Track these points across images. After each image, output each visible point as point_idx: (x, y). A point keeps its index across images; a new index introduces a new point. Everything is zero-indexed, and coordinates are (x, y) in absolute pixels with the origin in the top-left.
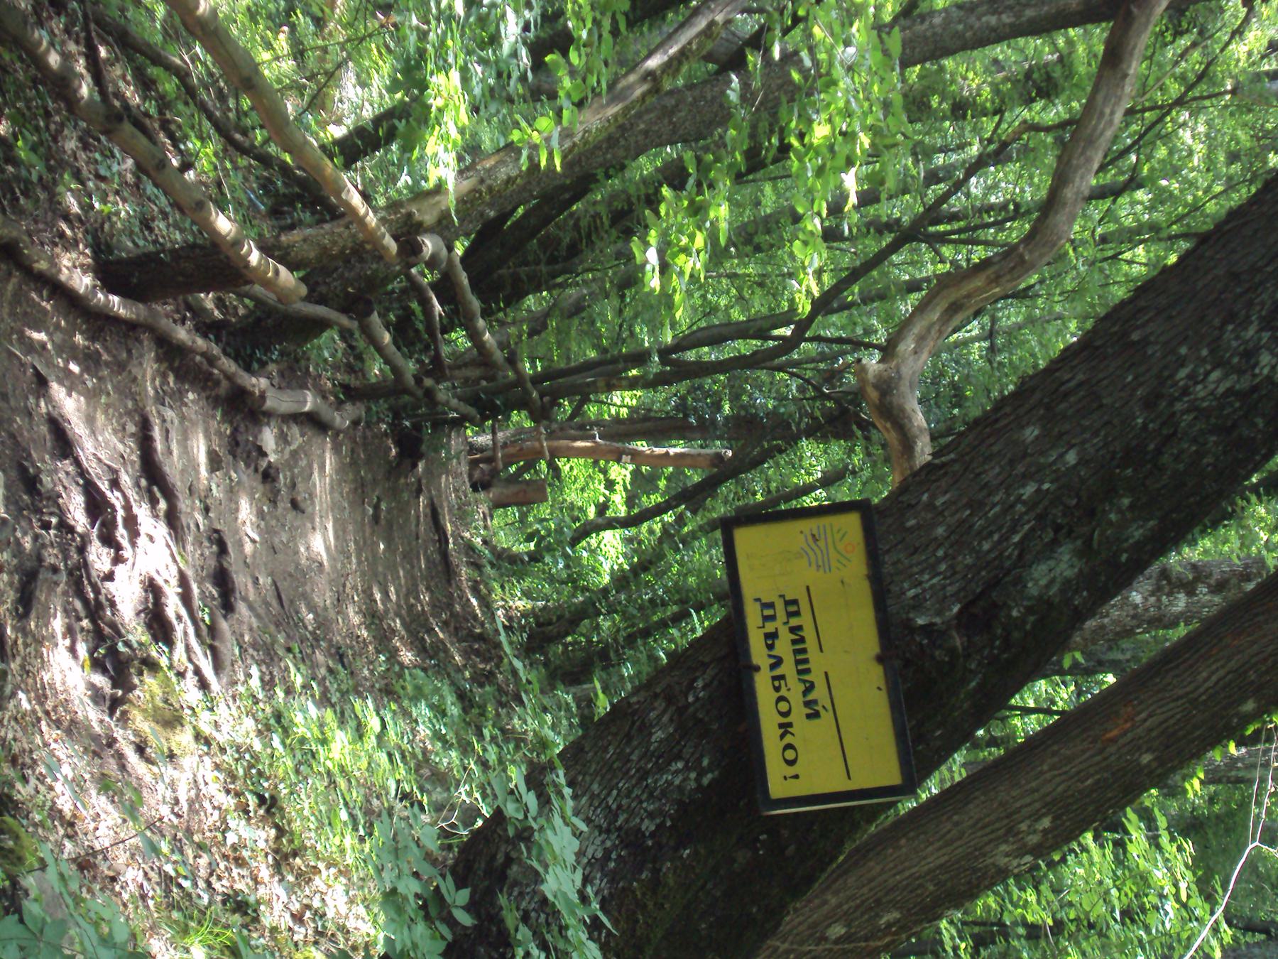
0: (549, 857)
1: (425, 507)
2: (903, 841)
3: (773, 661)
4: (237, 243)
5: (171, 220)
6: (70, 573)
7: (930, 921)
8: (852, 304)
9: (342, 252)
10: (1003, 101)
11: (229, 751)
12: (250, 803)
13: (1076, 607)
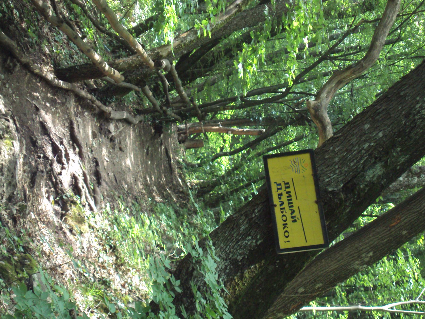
0: (206, 270)
1: (163, 149)
2: (323, 260)
3: (281, 203)
4: (101, 63)
5: (79, 55)
6: (47, 173)
7: (332, 287)
8: (305, 81)
9: (136, 66)
10: (355, 12)
11: (100, 231)
12: (107, 248)
13: (382, 184)
